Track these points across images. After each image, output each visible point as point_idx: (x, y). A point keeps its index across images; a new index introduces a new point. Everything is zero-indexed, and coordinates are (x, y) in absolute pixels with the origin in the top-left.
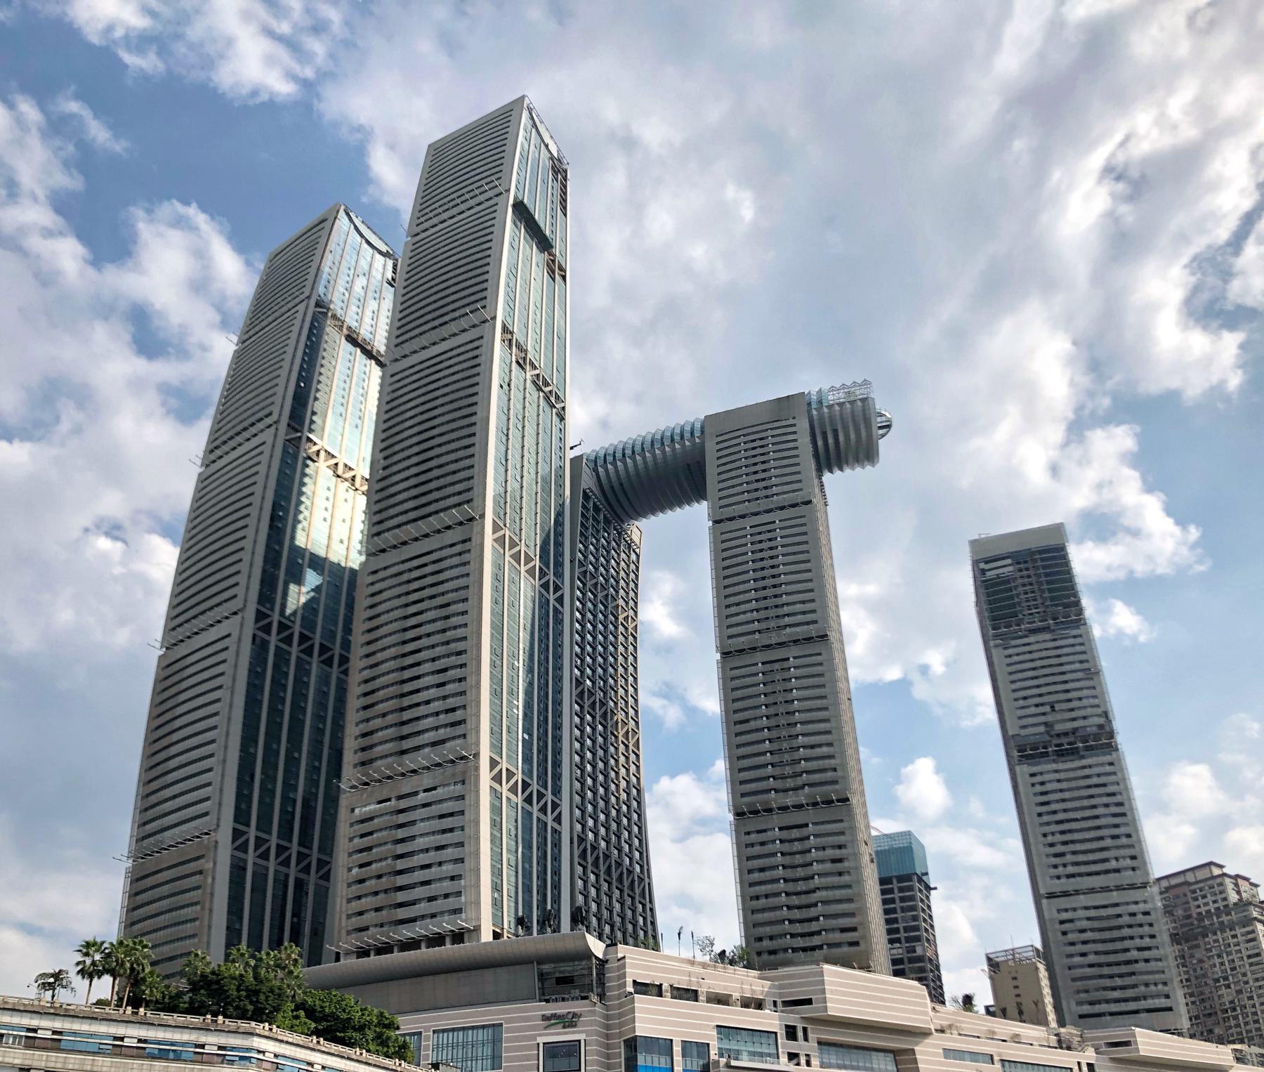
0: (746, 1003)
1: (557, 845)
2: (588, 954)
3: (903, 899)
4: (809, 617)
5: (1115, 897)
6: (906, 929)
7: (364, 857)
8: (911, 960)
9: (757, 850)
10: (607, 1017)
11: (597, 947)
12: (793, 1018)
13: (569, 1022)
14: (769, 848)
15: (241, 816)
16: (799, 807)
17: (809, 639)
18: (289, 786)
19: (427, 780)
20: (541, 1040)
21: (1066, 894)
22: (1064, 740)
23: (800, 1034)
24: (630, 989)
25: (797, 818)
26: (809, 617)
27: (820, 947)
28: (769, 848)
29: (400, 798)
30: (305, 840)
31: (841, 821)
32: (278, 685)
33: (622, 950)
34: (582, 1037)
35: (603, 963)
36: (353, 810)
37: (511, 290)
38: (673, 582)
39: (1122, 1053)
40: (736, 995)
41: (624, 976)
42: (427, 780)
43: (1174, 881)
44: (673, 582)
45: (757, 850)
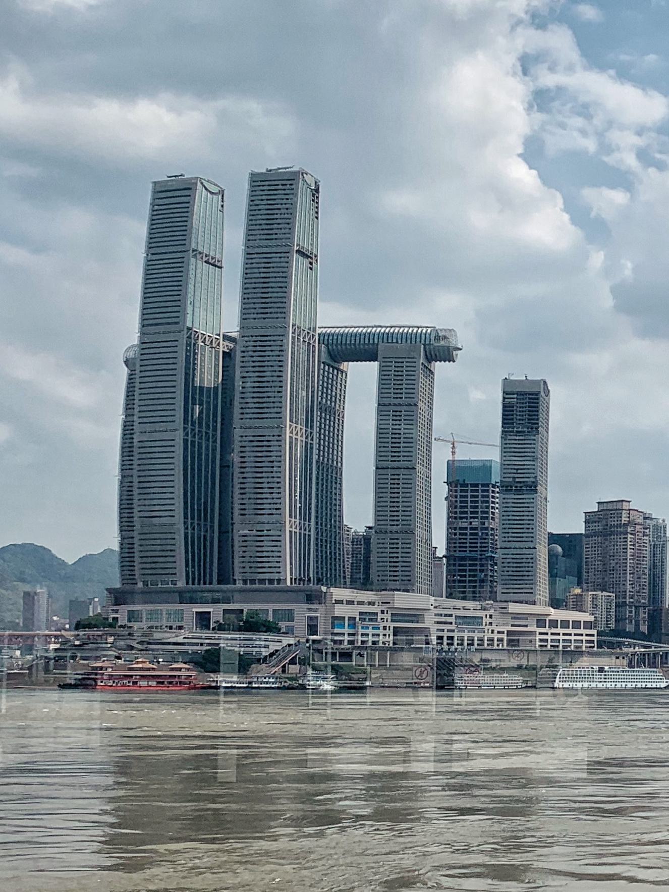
0: (370, 603)
1: (309, 540)
3: (483, 496)
4: (409, 459)
5: (525, 551)
6: (482, 512)
8: (482, 529)
11: (324, 589)
12: (384, 608)
13: (316, 610)
14: (385, 546)
15: (186, 517)
16: (397, 532)
17: (408, 468)
18: (199, 499)
19: (267, 527)
21: (506, 548)
22: (519, 485)
25: (396, 536)
26: (409, 459)
28: (385, 546)
30: (206, 520)
32: (193, 458)
33: (332, 590)
38: (362, 380)
39: (504, 611)
42: (267, 527)
43: (610, 507)
44: (362, 380)
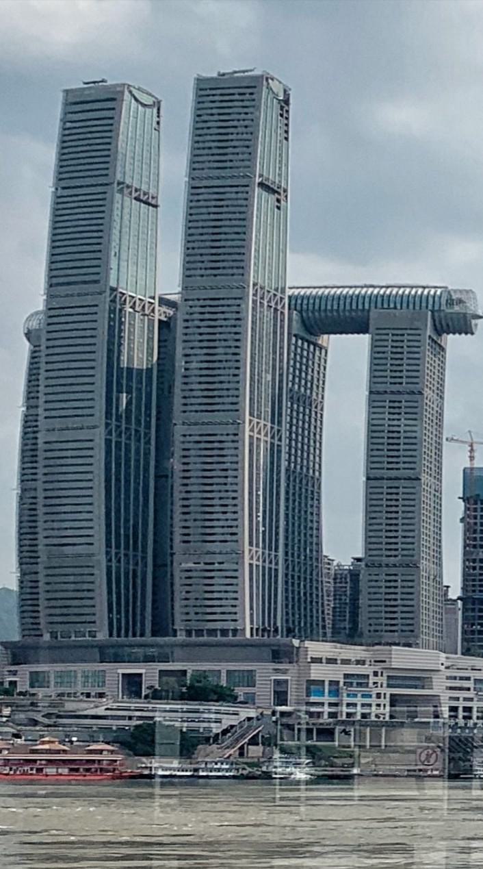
0: (358, 662)
2: (293, 646)
4: (412, 466)
7: (188, 588)
9: (373, 584)
10: (299, 670)
11: (296, 642)
12: (378, 668)
13: (285, 672)
15: (108, 545)
17: (410, 479)
19: (219, 558)
20: (273, 678)
23: (380, 674)
24: (309, 660)
25: (393, 571)
26: (412, 466)
27: (397, 631)
29: (206, 564)
30: (135, 549)
31: (413, 575)
33: (307, 644)
34: (289, 678)
35: (298, 648)
36: (181, 564)
37: (257, 251)
40: (353, 659)
41: (307, 655)
42: (219, 558)
45: (373, 584)
